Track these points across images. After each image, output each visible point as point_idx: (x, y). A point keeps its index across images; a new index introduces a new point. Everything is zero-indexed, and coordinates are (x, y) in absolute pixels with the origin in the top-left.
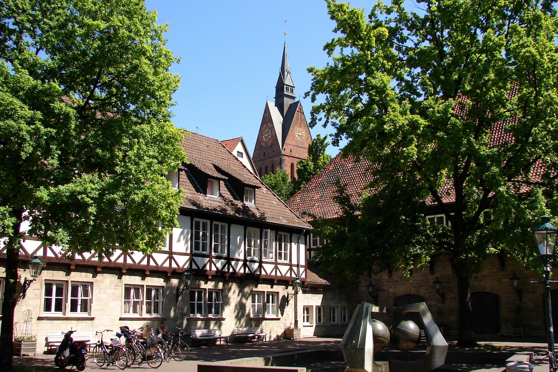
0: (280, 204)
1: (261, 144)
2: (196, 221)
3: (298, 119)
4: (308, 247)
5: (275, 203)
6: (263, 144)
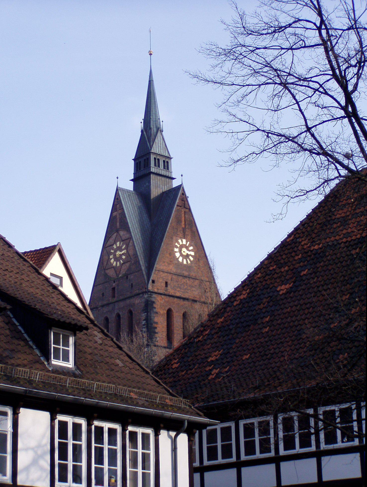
0: (131, 366)
1: (107, 271)
2: (60, 422)
3: (178, 221)
4: (197, 464)
5: (121, 364)
6: (111, 273)
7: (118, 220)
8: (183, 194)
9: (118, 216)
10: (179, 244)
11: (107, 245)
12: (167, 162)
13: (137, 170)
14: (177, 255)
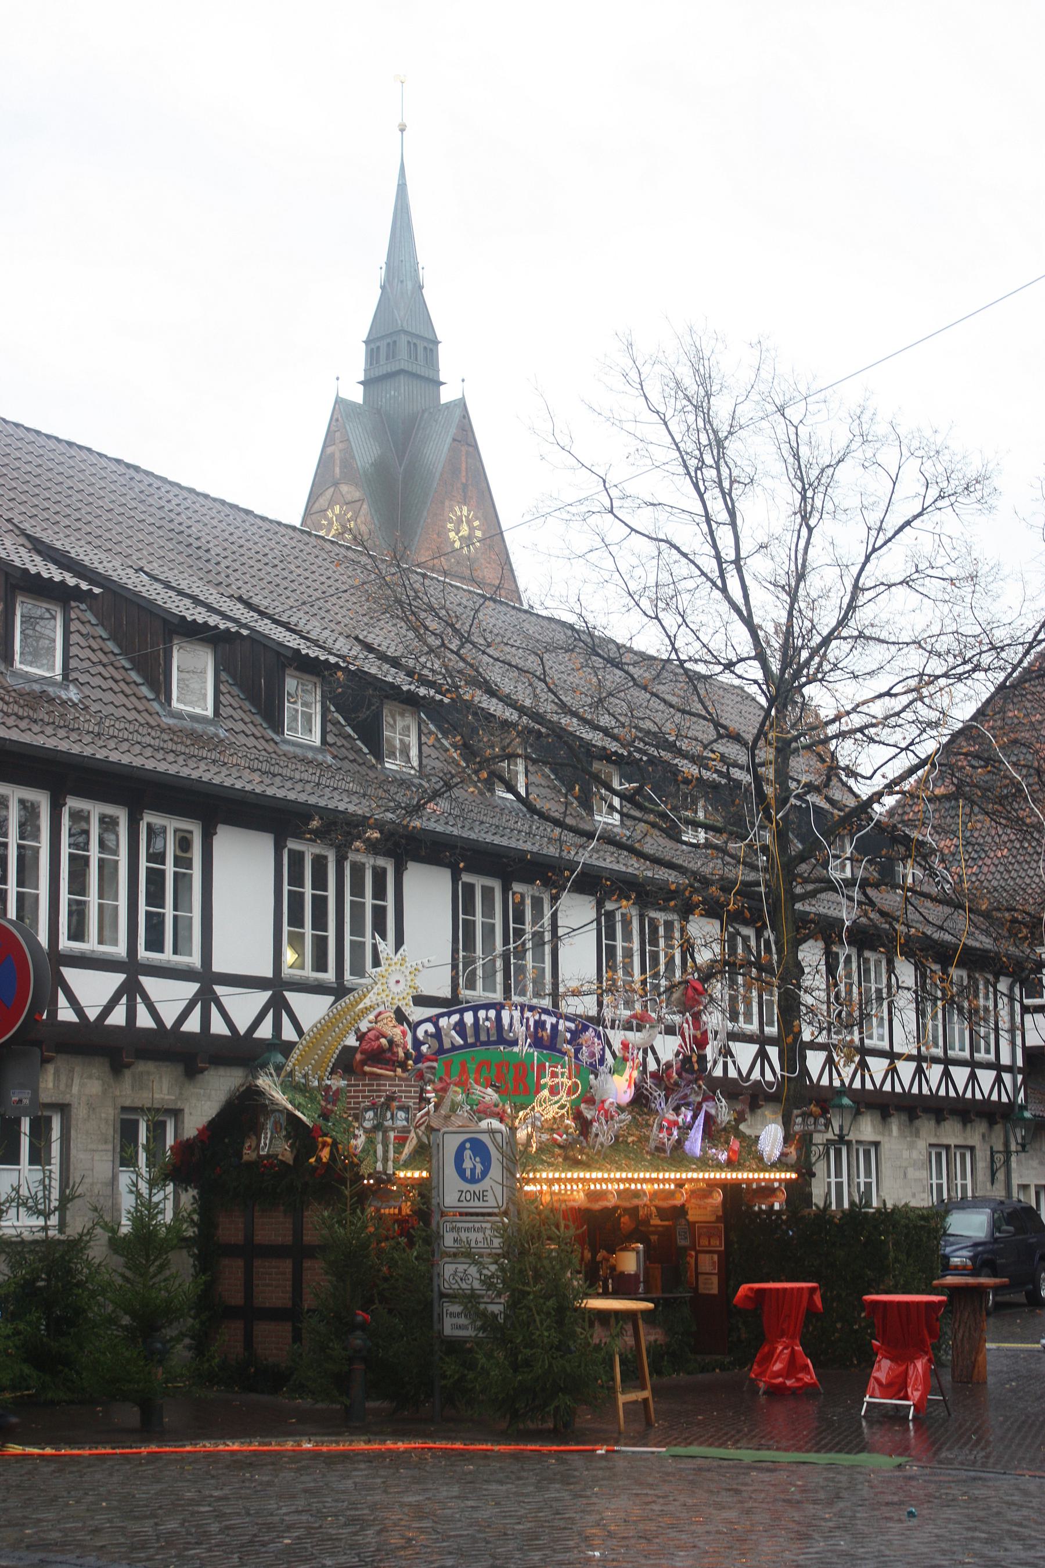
7: (338, 462)
8: (464, 417)
9: (337, 455)
10: (456, 515)
11: (314, 510)
12: (431, 350)
13: (371, 364)
14: (452, 535)
